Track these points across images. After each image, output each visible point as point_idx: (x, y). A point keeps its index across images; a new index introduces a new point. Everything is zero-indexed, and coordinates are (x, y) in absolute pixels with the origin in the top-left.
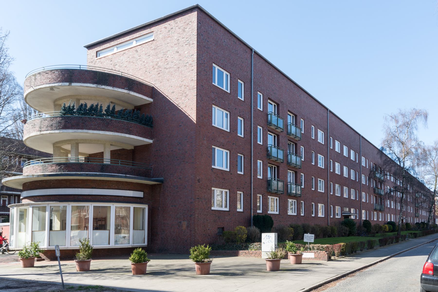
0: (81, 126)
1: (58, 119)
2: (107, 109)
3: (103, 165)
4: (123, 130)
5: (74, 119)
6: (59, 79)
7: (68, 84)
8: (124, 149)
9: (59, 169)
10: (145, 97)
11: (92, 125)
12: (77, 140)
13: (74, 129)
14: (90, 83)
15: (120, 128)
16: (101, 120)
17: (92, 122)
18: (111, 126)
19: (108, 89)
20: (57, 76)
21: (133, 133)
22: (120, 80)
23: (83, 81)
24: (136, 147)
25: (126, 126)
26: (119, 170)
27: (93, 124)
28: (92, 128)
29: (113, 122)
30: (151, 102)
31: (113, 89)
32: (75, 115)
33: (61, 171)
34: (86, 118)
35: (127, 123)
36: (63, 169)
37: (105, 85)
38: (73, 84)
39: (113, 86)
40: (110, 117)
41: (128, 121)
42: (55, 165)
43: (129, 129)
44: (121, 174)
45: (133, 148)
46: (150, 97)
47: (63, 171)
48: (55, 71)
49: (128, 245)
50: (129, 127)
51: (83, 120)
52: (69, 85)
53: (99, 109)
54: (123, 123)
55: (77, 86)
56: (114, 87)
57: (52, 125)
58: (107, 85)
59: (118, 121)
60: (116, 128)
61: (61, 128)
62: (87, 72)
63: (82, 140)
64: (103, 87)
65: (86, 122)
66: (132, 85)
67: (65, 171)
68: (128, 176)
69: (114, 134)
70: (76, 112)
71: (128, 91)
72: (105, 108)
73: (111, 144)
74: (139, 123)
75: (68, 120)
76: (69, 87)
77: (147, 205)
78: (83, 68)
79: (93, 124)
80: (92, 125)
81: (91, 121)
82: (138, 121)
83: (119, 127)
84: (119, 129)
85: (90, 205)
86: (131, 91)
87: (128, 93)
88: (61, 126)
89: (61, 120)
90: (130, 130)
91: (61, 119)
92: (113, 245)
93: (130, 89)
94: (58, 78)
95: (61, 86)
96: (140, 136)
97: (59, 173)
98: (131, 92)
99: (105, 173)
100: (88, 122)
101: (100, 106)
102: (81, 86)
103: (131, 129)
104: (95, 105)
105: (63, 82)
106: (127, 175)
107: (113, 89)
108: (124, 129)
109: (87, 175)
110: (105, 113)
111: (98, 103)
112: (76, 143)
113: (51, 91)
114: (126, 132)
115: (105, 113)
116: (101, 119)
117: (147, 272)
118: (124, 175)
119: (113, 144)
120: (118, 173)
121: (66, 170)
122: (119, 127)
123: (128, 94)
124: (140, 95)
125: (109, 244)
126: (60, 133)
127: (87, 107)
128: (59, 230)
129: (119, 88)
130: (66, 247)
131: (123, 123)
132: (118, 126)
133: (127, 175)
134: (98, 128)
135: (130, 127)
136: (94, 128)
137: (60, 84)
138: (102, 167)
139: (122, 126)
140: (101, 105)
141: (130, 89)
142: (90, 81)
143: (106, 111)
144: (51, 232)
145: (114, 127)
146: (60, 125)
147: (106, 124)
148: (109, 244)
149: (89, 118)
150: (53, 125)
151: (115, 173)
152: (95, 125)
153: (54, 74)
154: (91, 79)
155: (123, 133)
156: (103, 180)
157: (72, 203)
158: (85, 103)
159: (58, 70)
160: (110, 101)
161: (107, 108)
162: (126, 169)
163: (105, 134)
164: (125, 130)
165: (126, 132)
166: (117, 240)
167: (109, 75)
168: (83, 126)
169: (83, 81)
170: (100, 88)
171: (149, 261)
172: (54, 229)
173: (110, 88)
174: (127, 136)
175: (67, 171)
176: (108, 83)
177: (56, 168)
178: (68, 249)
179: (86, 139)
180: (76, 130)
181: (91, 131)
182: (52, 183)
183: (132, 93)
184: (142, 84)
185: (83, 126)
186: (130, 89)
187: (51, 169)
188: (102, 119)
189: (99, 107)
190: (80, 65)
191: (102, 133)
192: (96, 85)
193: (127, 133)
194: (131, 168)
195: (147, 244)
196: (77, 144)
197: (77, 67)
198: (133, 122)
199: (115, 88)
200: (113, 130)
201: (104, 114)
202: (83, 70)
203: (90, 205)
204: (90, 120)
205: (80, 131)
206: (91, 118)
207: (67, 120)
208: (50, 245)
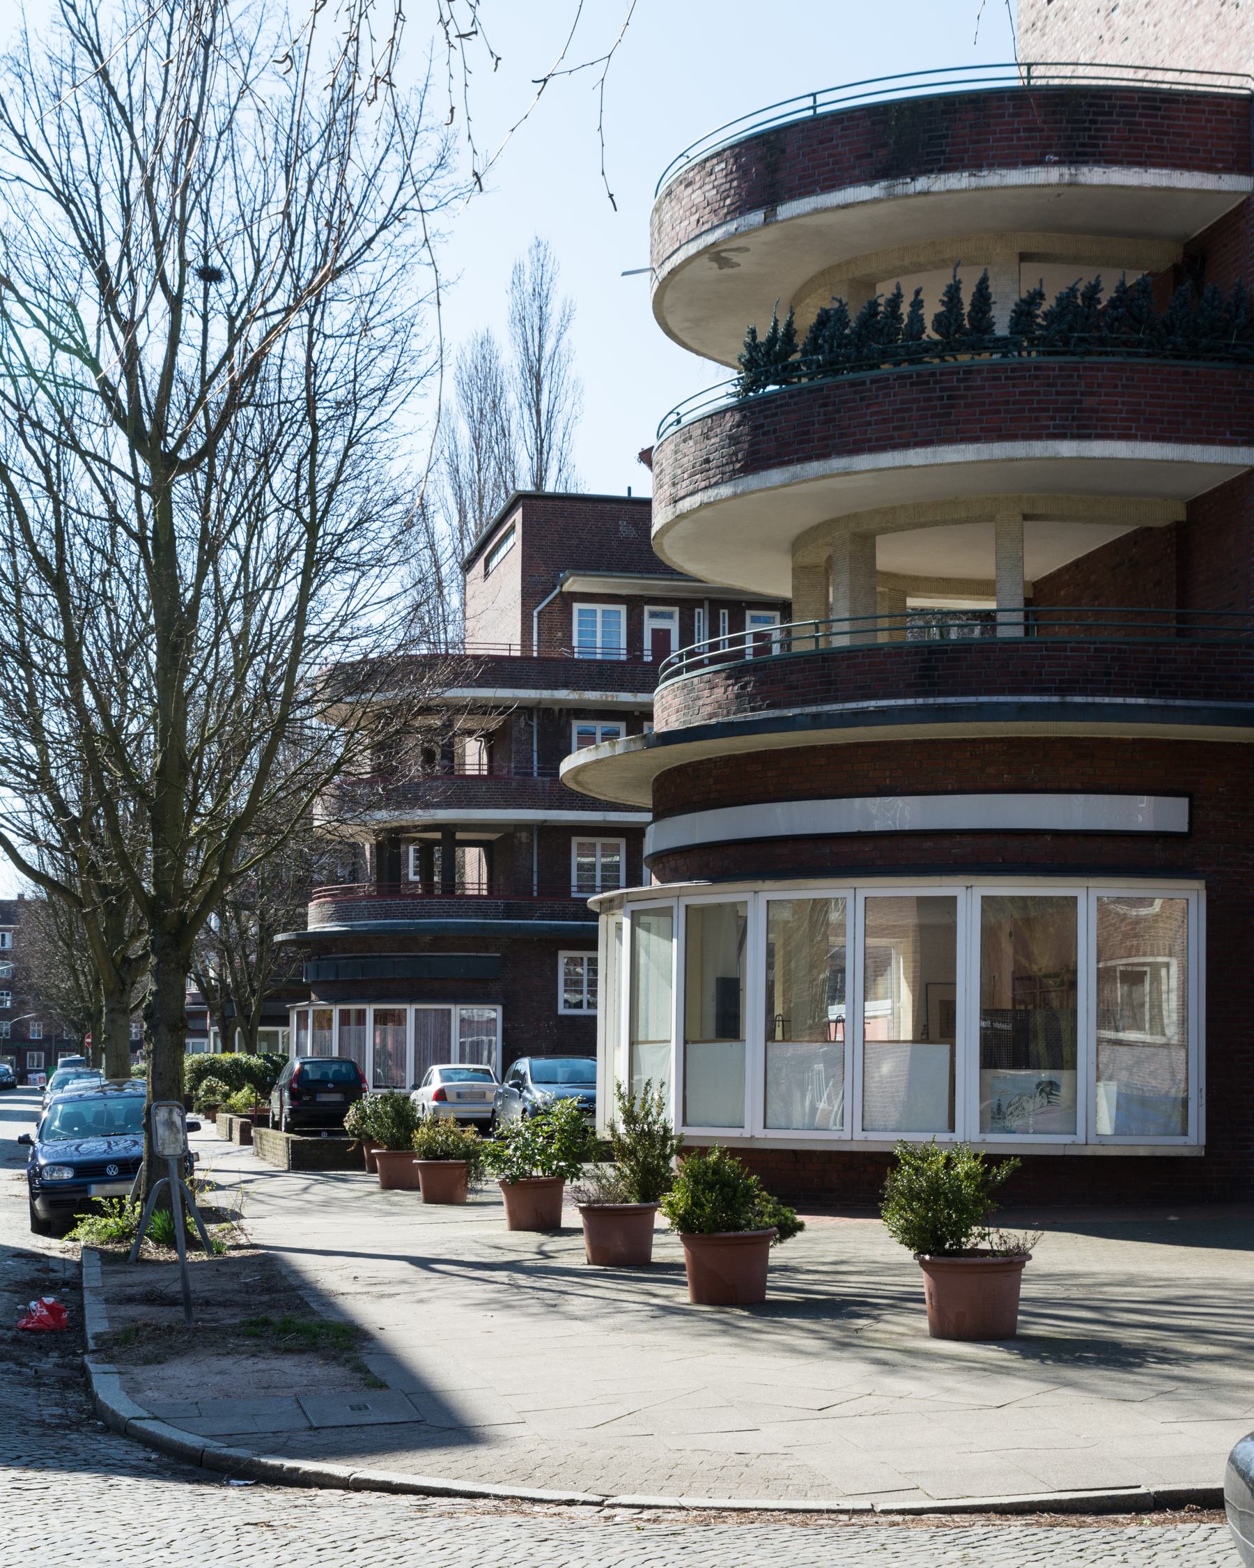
0: (820, 439)
1: (730, 421)
2: (943, 309)
3: (930, 652)
4: (1037, 419)
5: (787, 404)
6: (728, 202)
7: (757, 217)
8: (1151, 529)
9: (738, 696)
10: (1187, 174)
11: (869, 424)
12: (855, 516)
13: (790, 462)
14: (855, 181)
15: (1023, 411)
16: (912, 384)
17: (868, 406)
18: (966, 406)
19: (949, 191)
20: (723, 188)
21: (1106, 428)
22: (1015, 115)
23: (825, 180)
24: (1194, 505)
25: (1058, 393)
26: (1024, 673)
27: (872, 414)
28: (869, 440)
29: (979, 383)
30: (1244, 197)
31: (974, 182)
32: (795, 380)
33: (745, 711)
34: (837, 387)
35: (1061, 369)
36: (752, 697)
37: (931, 171)
38: (786, 210)
39: (976, 164)
40: (964, 358)
41: (1073, 354)
42: (723, 675)
43: (1080, 402)
44: (1035, 692)
45: (1182, 516)
46: (1229, 170)
47: (753, 709)
48: (715, 161)
49: (1180, 1140)
50: (1074, 393)
51: (825, 405)
52: (767, 222)
53: (906, 321)
54: (1037, 377)
55: (799, 216)
56: (980, 167)
57: (707, 461)
58: (943, 170)
59: (1005, 370)
60: (998, 412)
61: (741, 470)
62: (841, 121)
63: (877, 511)
64: (922, 183)
65: (838, 411)
66: (1093, 122)
67: (760, 709)
68: (1078, 699)
69: (986, 457)
70: (799, 363)
71: (1065, 170)
72: (932, 309)
73: (1029, 511)
74: (1148, 355)
75: (766, 417)
76: (770, 233)
77: (1203, 882)
78: (830, 103)
79: (872, 414)
80: (869, 424)
81: (862, 399)
82: (1140, 343)
83: (1015, 403)
84: (1012, 420)
85: (1080, 893)
86: (1085, 163)
87: (1067, 178)
88: (740, 456)
89: (738, 426)
90: (1080, 410)
91: (737, 417)
92: (975, 1136)
93: (1078, 154)
94: (725, 199)
95: (736, 235)
96: (1157, 438)
97: (740, 717)
98: (1085, 170)
99: (941, 700)
100: (850, 409)
101: (912, 298)
102: (816, 211)
103: (1089, 402)
104: (1081, 287)
105: (742, 214)
106: (1069, 699)
107: (974, 182)
108: (1047, 410)
109: (817, 722)
110: (936, 337)
111: (898, 288)
112: (854, 534)
113: (727, 271)
114: (1055, 427)
115: (936, 337)
116: (910, 377)
117: (771, 1296)
118: (1055, 699)
119: (1040, 510)
120: (1013, 692)
121: (763, 700)
122: (1015, 403)
123: (1070, 184)
124: (1152, 171)
125: (953, 1131)
126: (735, 496)
127: (846, 325)
128: (947, 1047)
129: (1011, 162)
130: (746, 1133)
131: (1037, 377)
132: (1007, 402)
133: (1069, 699)
134: (900, 437)
135: (1082, 394)
136: (877, 439)
137: (732, 227)
138: (924, 661)
139: (1030, 393)
140: (918, 293)
141: (1075, 156)
142: (857, 172)
143: (939, 322)
144: (769, 1044)
145: (982, 413)
146: (735, 453)
147: (938, 403)
148: (952, 1128)
149: (853, 384)
150: (711, 457)
151: (1000, 692)
152: (885, 421)
153: (713, 177)
154: (858, 158)
155: (1039, 437)
156: (932, 742)
157: (769, 884)
158: (836, 305)
159: (724, 150)
160: (1018, 251)
161: (943, 303)
162: (1067, 658)
163: (939, 461)
164: (1053, 419)
165: (1055, 427)
166: (1004, 1109)
167: (953, 103)
168: (825, 438)
169: (825, 180)
170: (907, 196)
171: (789, 1230)
172: (647, 1035)
173: (958, 181)
174: (1067, 449)
175: (769, 707)
176: (943, 152)
177: (726, 691)
178: (758, 1145)
179: (893, 508)
180: (797, 469)
181: (864, 462)
182: (711, 781)
183: (1095, 176)
184: (1163, 100)
185: (825, 438)
186: (1078, 154)
187: (708, 701)
188: (919, 375)
189: (905, 309)
190: (814, 95)
191: (921, 462)
192: (883, 184)
193: (1062, 436)
194: (1096, 650)
195: (1203, 1141)
196: (864, 543)
197: (799, 111)
198: (1107, 353)
199: (985, 173)
200: (982, 430)
201: (931, 347)
202: (1048, 88)
203: (1080, 893)
204: (858, 397)
205: (815, 467)
206: (864, 383)
207: (762, 421)
208: (769, 1121)
